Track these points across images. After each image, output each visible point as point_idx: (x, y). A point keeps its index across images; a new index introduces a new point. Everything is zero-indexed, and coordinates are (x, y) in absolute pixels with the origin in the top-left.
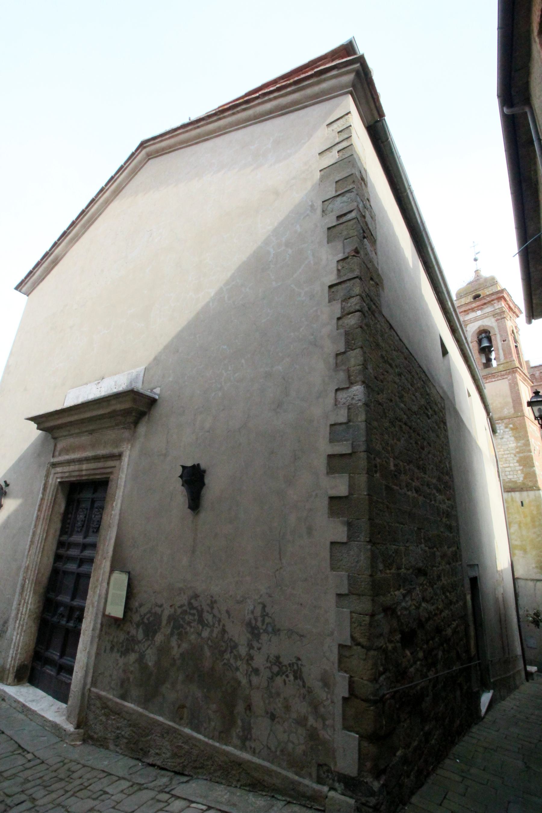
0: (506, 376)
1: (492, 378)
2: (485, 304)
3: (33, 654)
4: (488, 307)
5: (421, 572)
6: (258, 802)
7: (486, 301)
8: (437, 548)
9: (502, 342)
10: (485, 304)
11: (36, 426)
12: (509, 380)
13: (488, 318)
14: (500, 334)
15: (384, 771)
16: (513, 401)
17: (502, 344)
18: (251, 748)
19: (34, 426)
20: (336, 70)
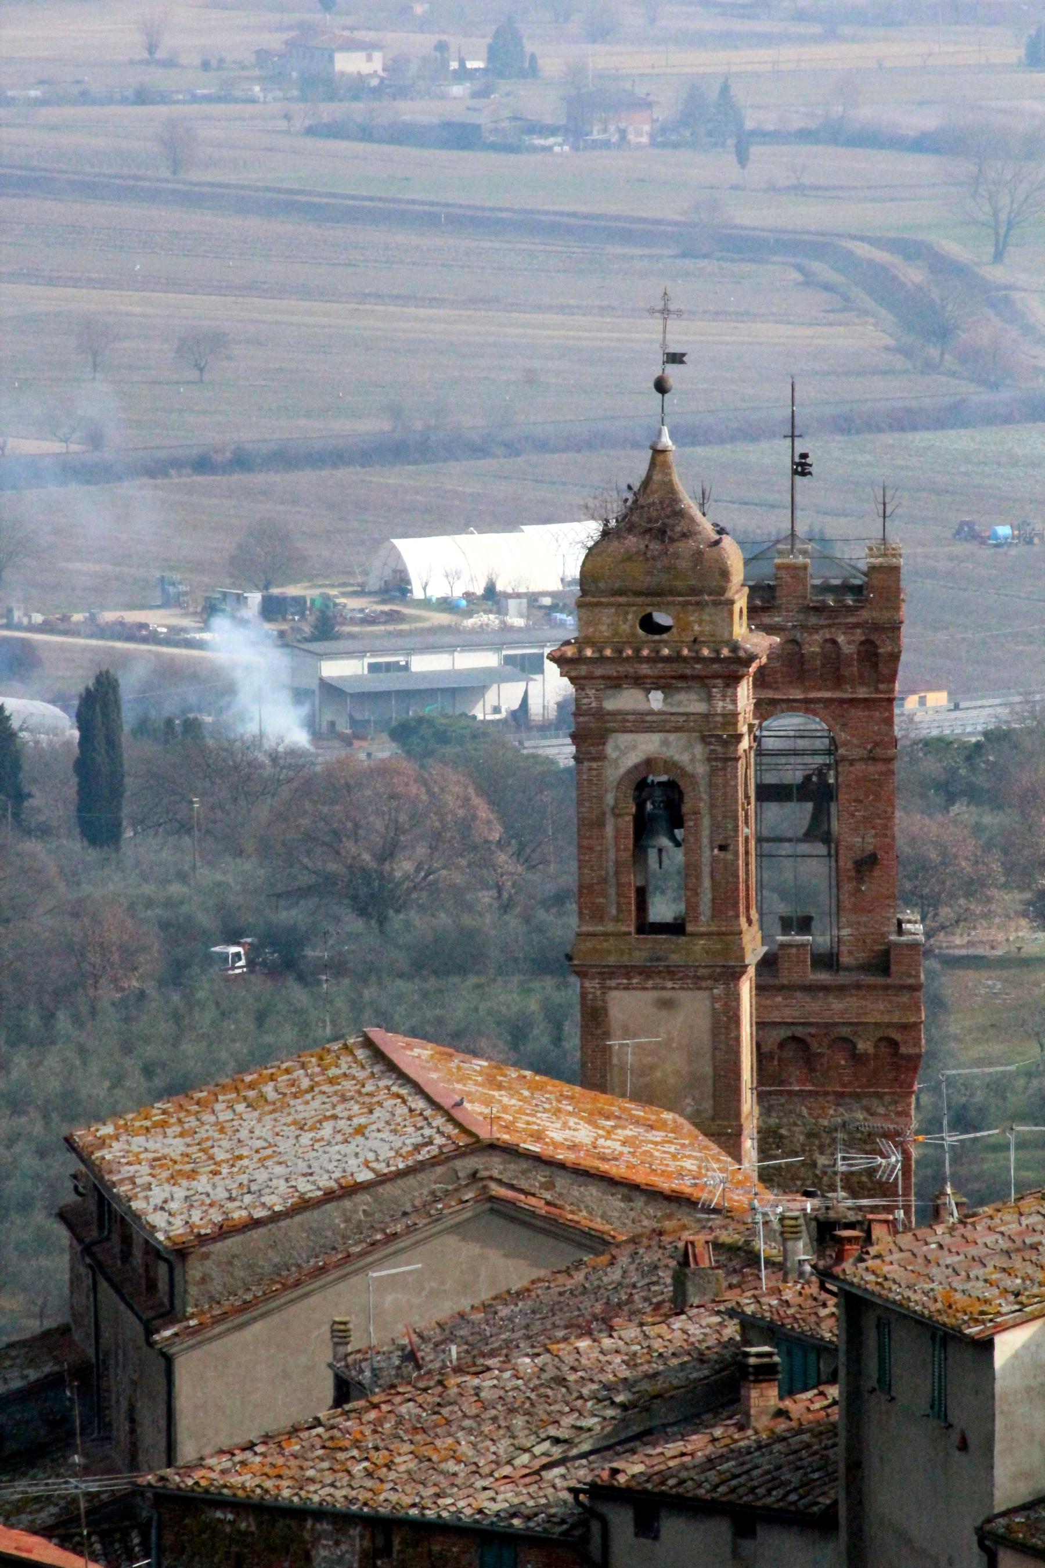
0: (709, 983)
1: (664, 979)
2: (683, 677)
3: (912, 133)
4: (689, 687)
5: (287, 1180)
6: (135, 983)
7: (688, 672)
8: (365, 1360)
9: (716, 851)
10: (683, 677)
11: (558, 670)
12: (714, 999)
13: (684, 735)
14: (713, 817)
15: (185, 732)
16: (716, 1077)
17: (714, 860)
18: (138, 864)
19: (515, 705)
20: (177, 611)
